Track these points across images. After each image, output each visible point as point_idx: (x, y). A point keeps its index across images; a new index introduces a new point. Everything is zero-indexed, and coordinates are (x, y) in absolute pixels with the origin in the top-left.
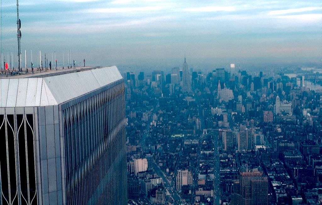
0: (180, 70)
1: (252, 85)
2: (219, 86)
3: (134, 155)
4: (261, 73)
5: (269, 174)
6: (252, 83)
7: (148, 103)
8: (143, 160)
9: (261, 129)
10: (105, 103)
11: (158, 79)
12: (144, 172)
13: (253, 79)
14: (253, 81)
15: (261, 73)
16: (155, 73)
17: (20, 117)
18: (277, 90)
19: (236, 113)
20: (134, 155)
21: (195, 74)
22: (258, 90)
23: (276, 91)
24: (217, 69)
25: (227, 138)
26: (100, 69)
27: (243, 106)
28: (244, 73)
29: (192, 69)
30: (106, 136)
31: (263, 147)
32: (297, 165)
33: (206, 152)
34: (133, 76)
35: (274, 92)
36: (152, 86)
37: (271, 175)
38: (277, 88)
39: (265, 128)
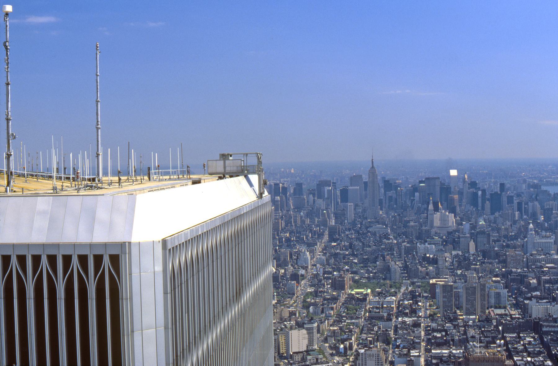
0: (364, 181)
1: (488, 204)
2: (431, 207)
3: (286, 323)
4: (502, 185)
5: (515, 358)
6: (487, 202)
7: (420, 206)
8: (301, 331)
9: (502, 280)
10: (239, 236)
11: (326, 196)
12: (302, 352)
13: (488, 196)
14: (488, 200)
15: (502, 185)
16: (323, 184)
17: (67, 259)
18: (530, 214)
19: (460, 253)
20: (286, 323)
21: (388, 185)
22: (497, 214)
23: (528, 216)
24: (428, 179)
25: (444, 297)
26: (222, 153)
27: (472, 240)
28: (473, 184)
29: (383, 178)
30: (238, 294)
31: (505, 311)
32: (318, 273)
33: (406, 319)
34: (285, 189)
35: (525, 217)
36: (316, 207)
37: (520, 360)
38: (530, 211)
39: (509, 278)
